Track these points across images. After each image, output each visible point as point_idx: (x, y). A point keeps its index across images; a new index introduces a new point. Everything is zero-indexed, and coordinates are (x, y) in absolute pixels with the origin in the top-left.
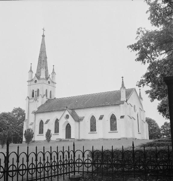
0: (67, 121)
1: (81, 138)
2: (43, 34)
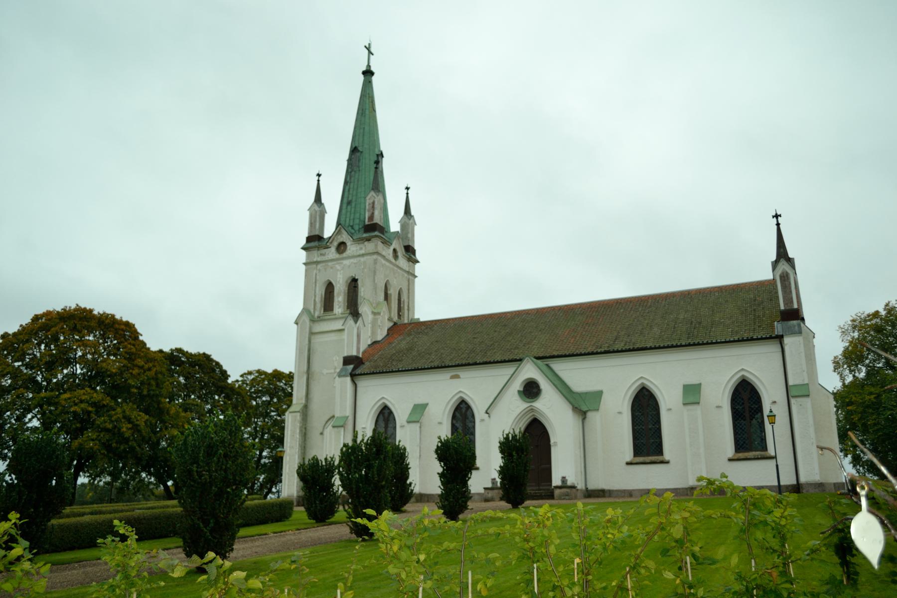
0: (532, 410)
1: (591, 486)
2: (369, 66)
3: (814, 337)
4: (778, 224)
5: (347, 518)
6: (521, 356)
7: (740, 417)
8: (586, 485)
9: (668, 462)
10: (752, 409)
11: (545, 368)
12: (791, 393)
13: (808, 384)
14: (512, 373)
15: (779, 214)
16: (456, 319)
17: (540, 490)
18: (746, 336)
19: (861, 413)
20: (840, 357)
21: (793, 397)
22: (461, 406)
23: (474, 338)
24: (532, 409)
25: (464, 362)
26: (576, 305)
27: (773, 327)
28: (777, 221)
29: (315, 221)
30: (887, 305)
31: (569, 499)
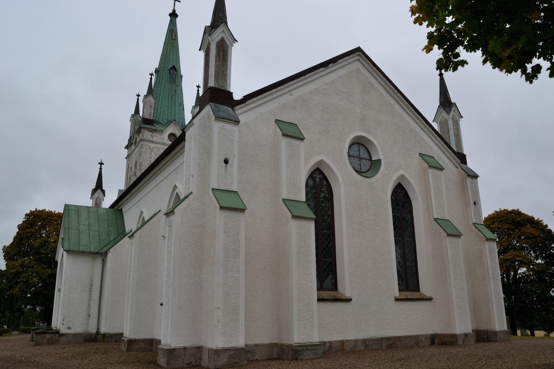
2: (174, 10)
4: (101, 169)
8: (98, 329)
9: (349, 300)
28: (101, 167)
29: (418, 117)
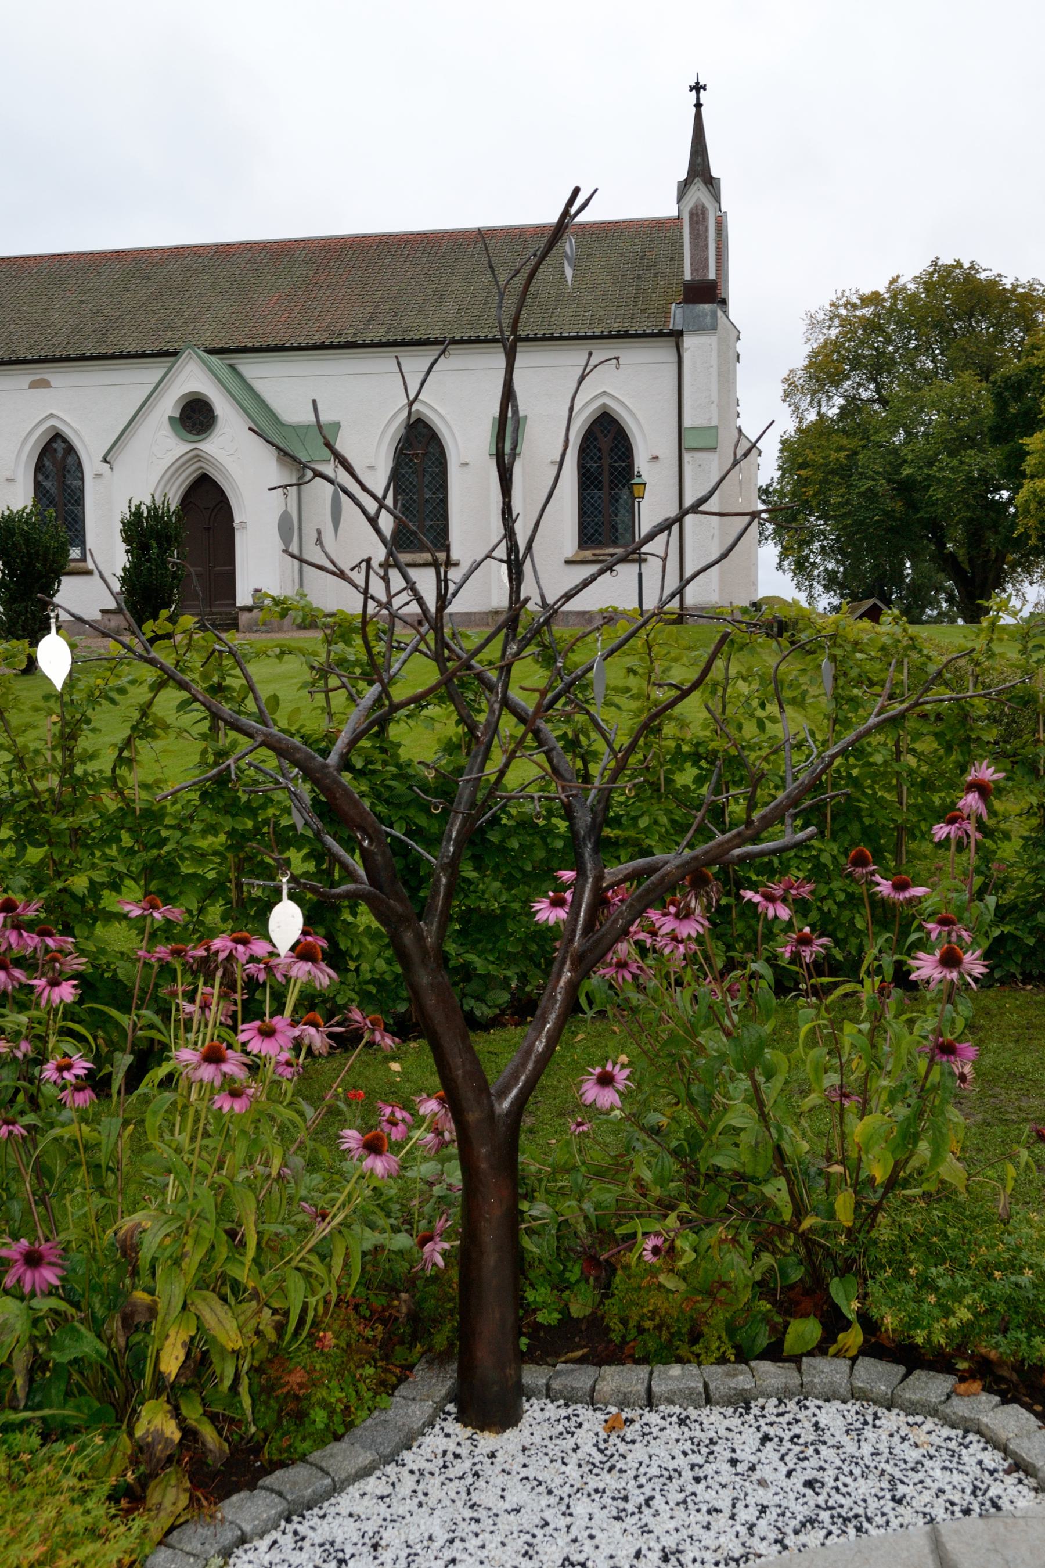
3: (738, 339)
4: (698, 106)
5: (302, 726)
6: (177, 345)
7: (592, 483)
10: (616, 469)
11: (225, 374)
12: (686, 444)
13: (716, 427)
14: (157, 380)
15: (702, 83)
16: (41, 257)
17: (213, 614)
18: (616, 327)
19: (821, 482)
20: (800, 373)
21: (688, 450)
22: (55, 445)
23: (82, 302)
24: (198, 456)
25: (58, 354)
26: (298, 241)
27: (667, 313)
28: (698, 98)
30: (894, 281)
31: (267, 632)
